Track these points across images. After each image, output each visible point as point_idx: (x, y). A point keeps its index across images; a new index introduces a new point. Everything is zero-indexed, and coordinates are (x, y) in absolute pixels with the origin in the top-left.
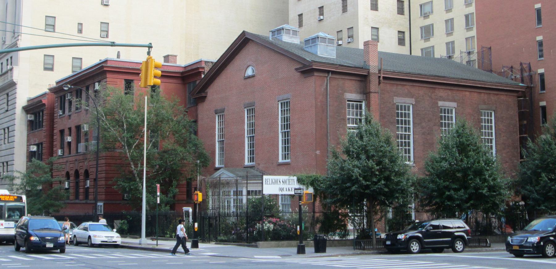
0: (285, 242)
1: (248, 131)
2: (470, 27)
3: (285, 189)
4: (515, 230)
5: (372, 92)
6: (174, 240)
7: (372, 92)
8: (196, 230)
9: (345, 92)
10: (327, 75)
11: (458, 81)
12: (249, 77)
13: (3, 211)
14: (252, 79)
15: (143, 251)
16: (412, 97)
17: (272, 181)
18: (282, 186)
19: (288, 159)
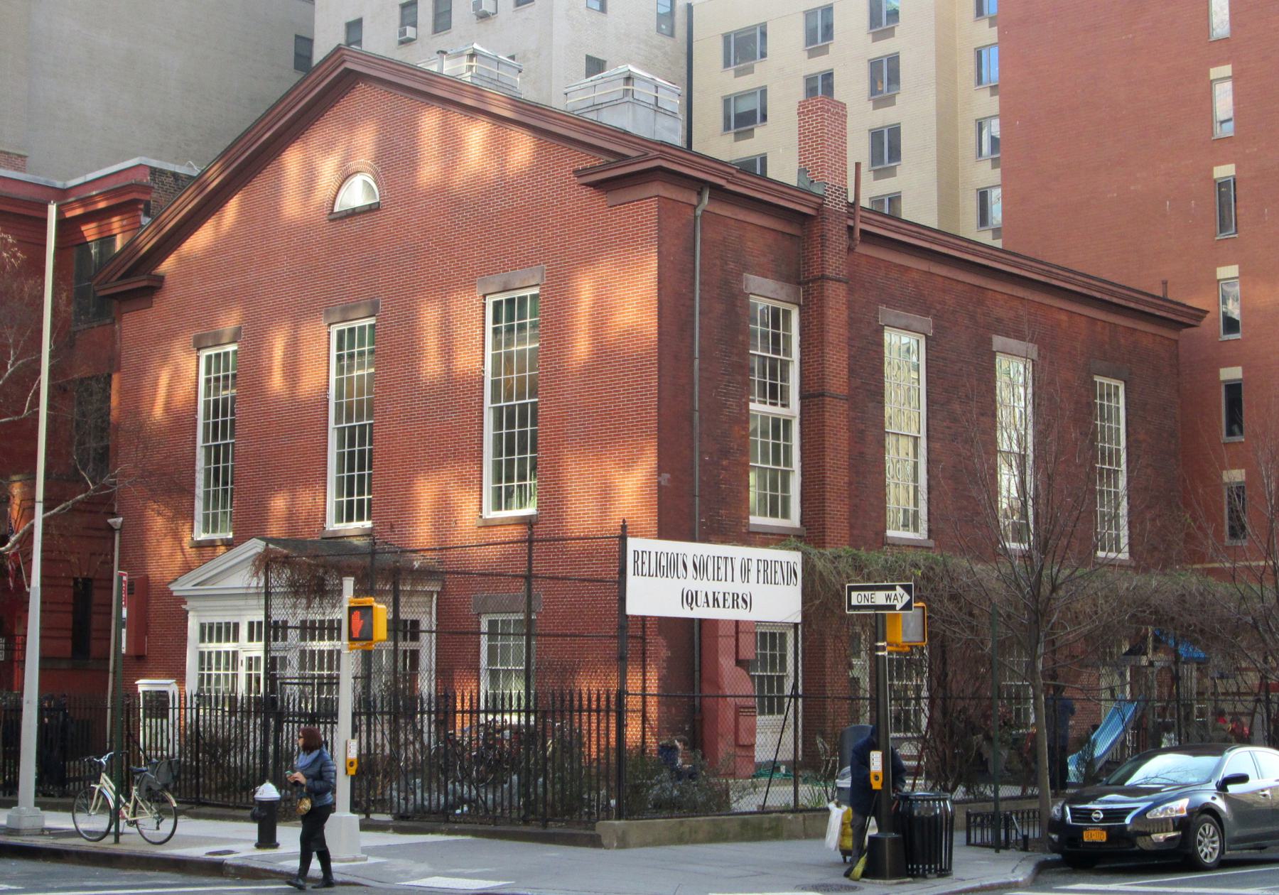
0: (661, 824)
1: (206, 426)
2: (887, 164)
3: (701, 599)
4: (662, 746)
5: (449, 371)
6: (297, 825)
7: (449, 371)
8: (873, 819)
9: (746, 268)
10: (694, 201)
11: (1049, 274)
12: (353, 213)
13: (1103, 509)
14: (376, 216)
15: (98, 871)
16: (927, 314)
17: (658, 563)
18: (692, 583)
19: (361, 518)
